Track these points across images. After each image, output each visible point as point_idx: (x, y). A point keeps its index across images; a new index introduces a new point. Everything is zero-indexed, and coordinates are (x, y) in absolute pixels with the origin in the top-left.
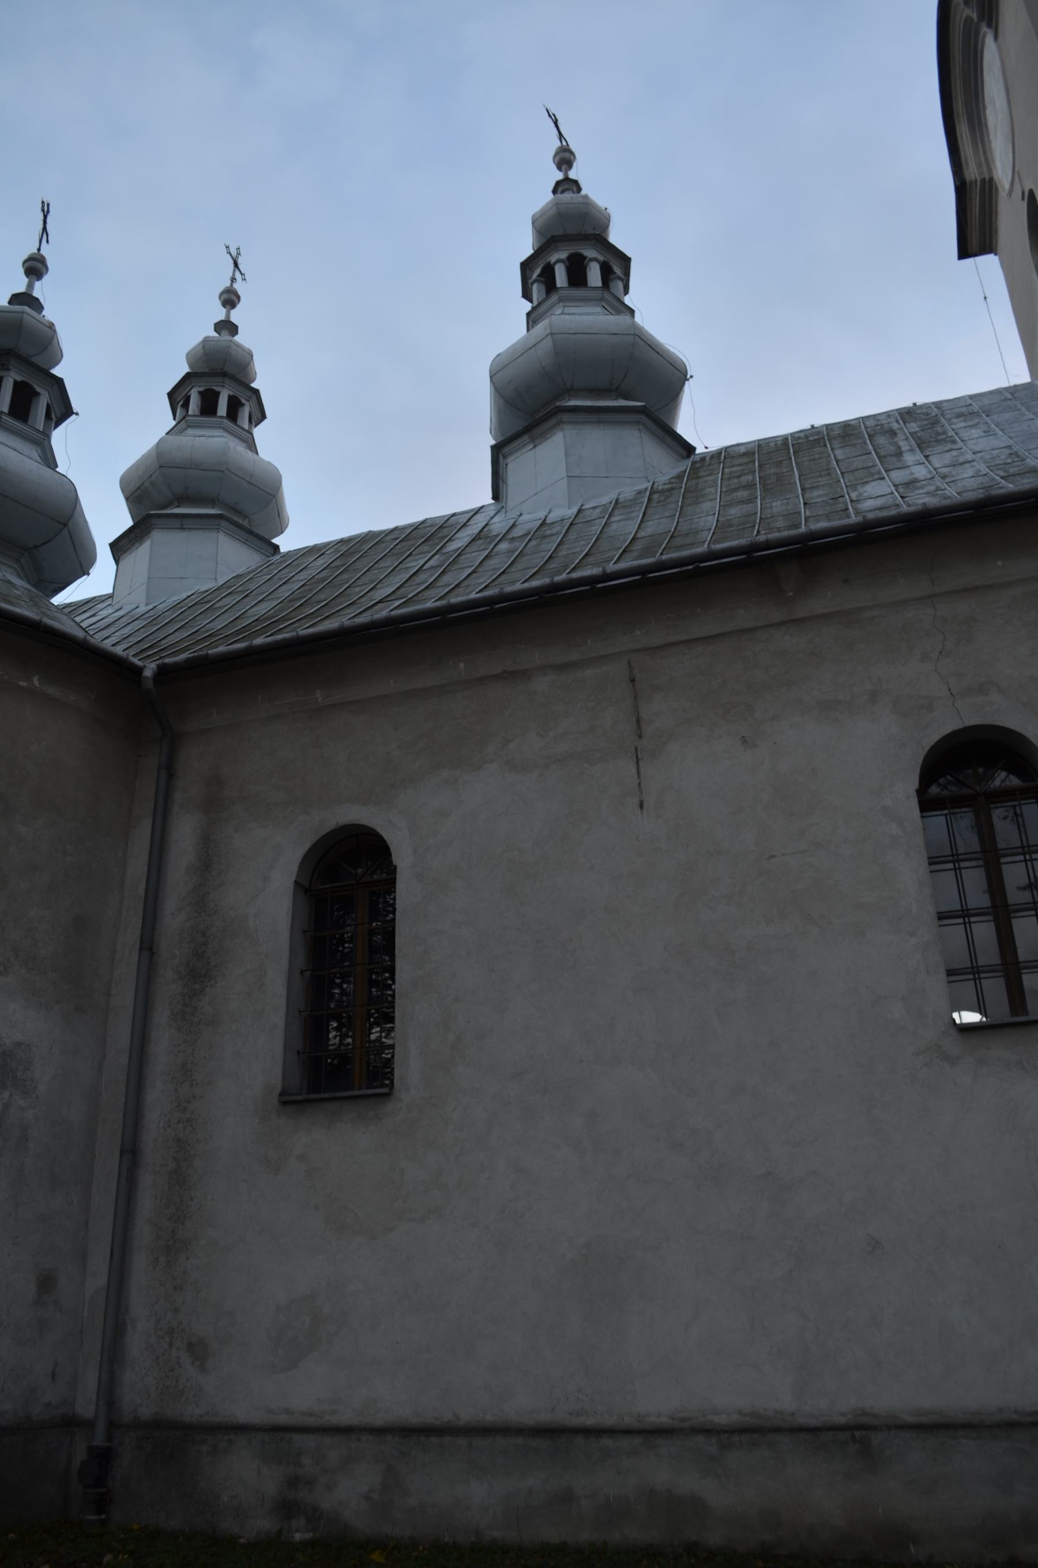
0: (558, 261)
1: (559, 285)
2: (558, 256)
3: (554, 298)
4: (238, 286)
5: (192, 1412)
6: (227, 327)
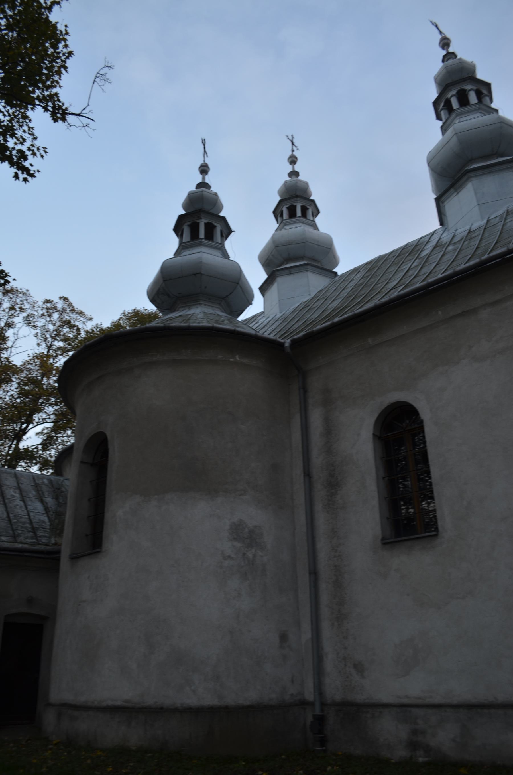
0: (452, 96)
1: (200, 237)
2: (452, 94)
3: (454, 115)
4: (296, 153)
5: (360, 698)
6: (294, 174)
